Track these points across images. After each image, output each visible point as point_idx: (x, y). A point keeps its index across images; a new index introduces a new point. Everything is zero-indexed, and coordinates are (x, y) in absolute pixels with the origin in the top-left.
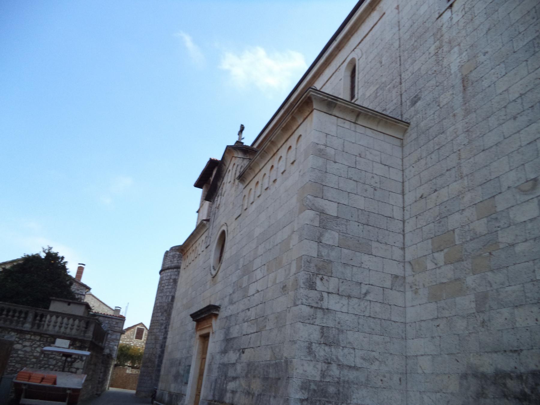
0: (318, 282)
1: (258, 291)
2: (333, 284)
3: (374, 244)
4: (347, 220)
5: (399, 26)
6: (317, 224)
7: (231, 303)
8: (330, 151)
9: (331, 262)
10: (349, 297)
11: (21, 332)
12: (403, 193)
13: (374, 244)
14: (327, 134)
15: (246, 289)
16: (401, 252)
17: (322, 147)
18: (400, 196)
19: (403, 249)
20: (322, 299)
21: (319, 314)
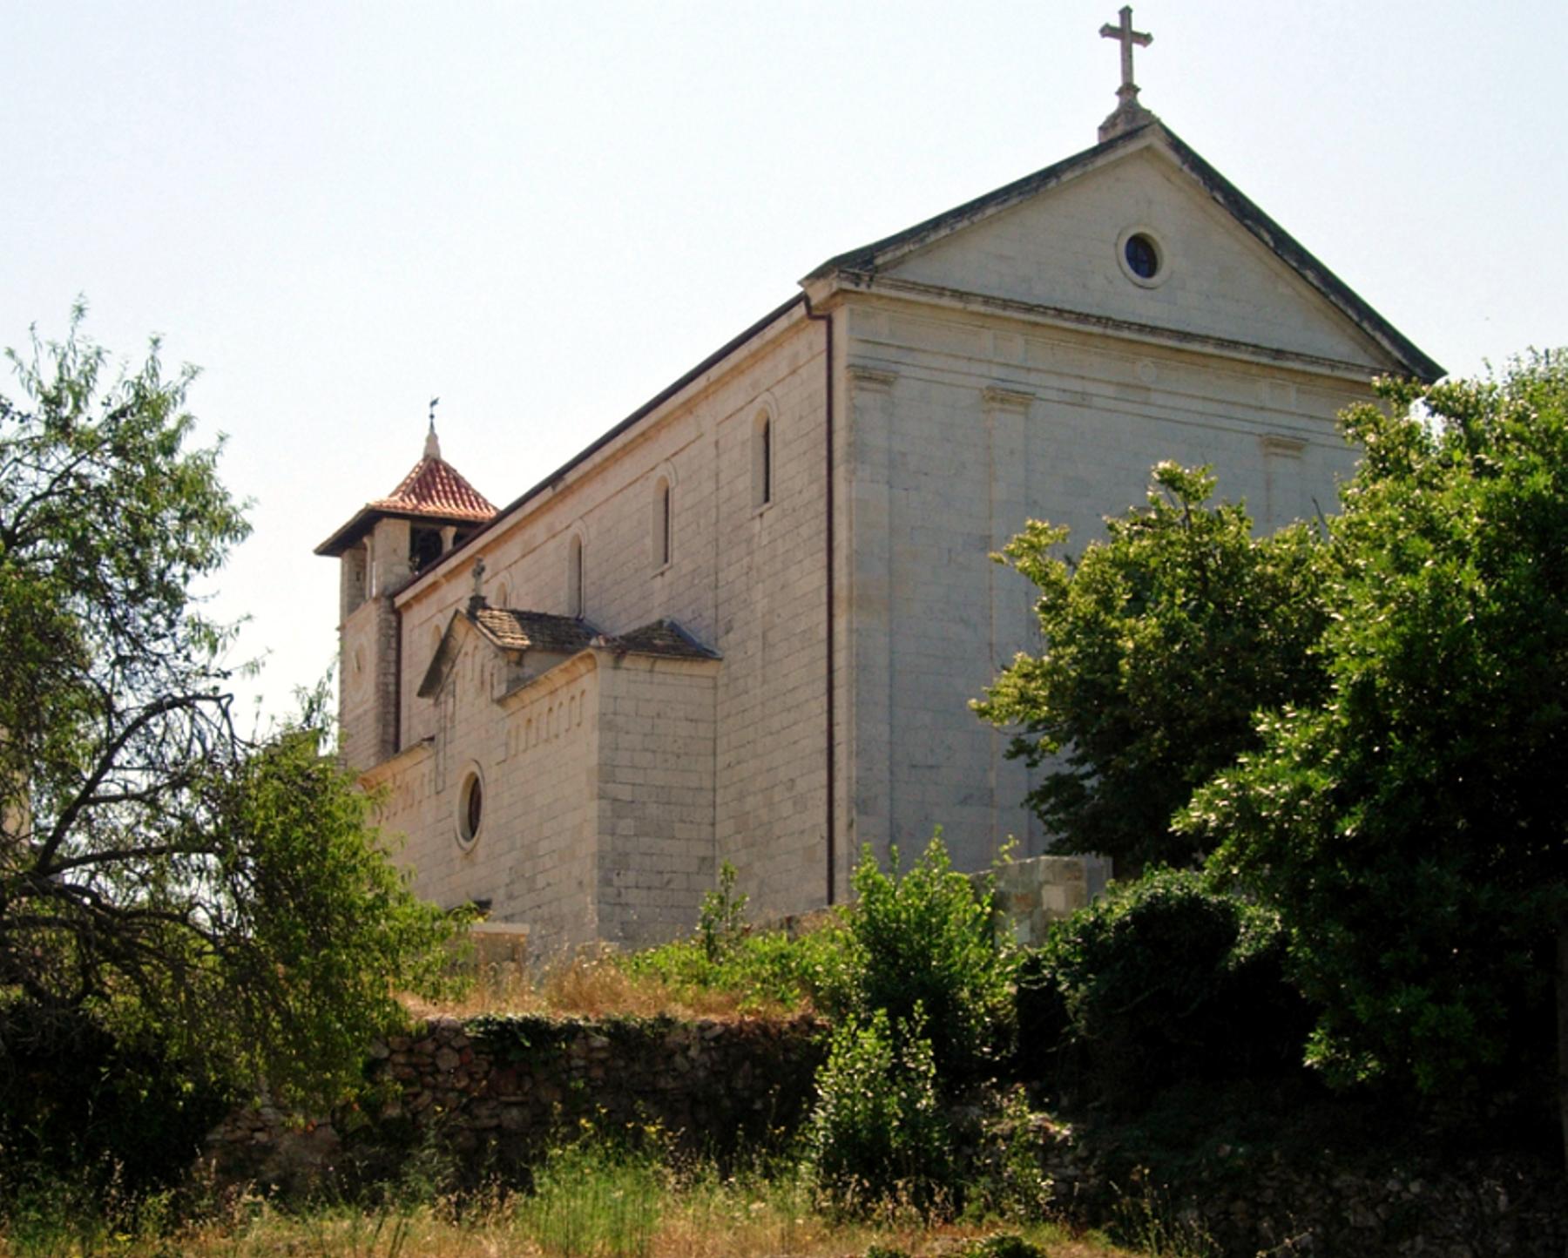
0: (615, 878)
1: (549, 885)
2: (631, 878)
3: (677, 825)
4: (644, 803)
5: (717, 482)
6: (609, 814)
7: (511, 897)
8: (620, 720)
9: (627, 854)
10: (649, 888)
11: (78, 946)
12: (715, 754)
13: (677, 825)
14: (616, 698)
15: (533, 879)
16: (710, 829)
17: (610, 717)
18: (711, 759)
19: (713, 825)
20: (619, 895)
21: (618, 909)
